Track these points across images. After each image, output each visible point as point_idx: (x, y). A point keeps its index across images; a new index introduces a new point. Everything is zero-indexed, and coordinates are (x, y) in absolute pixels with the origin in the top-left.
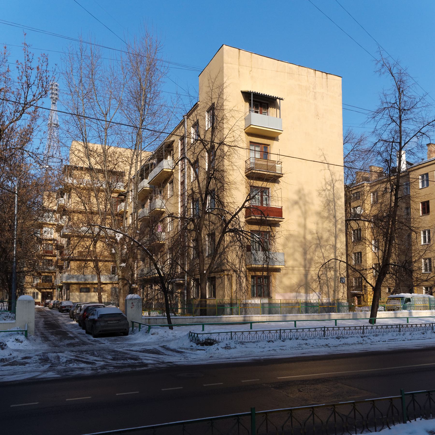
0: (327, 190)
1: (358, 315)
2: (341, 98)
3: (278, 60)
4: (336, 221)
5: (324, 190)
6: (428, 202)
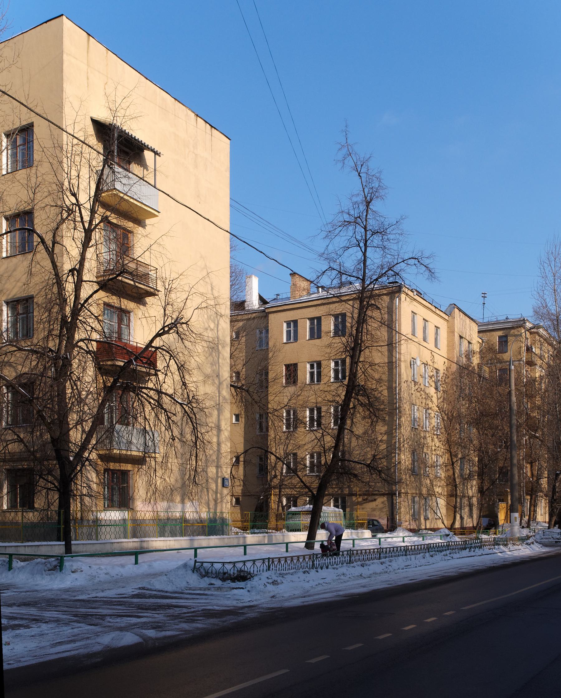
0: (209, 329)
1: (274, 537)
2: (228, 174)
3: (147, 79)
4: (220, 383)
5: (207, 329)
6: (295, 365)
